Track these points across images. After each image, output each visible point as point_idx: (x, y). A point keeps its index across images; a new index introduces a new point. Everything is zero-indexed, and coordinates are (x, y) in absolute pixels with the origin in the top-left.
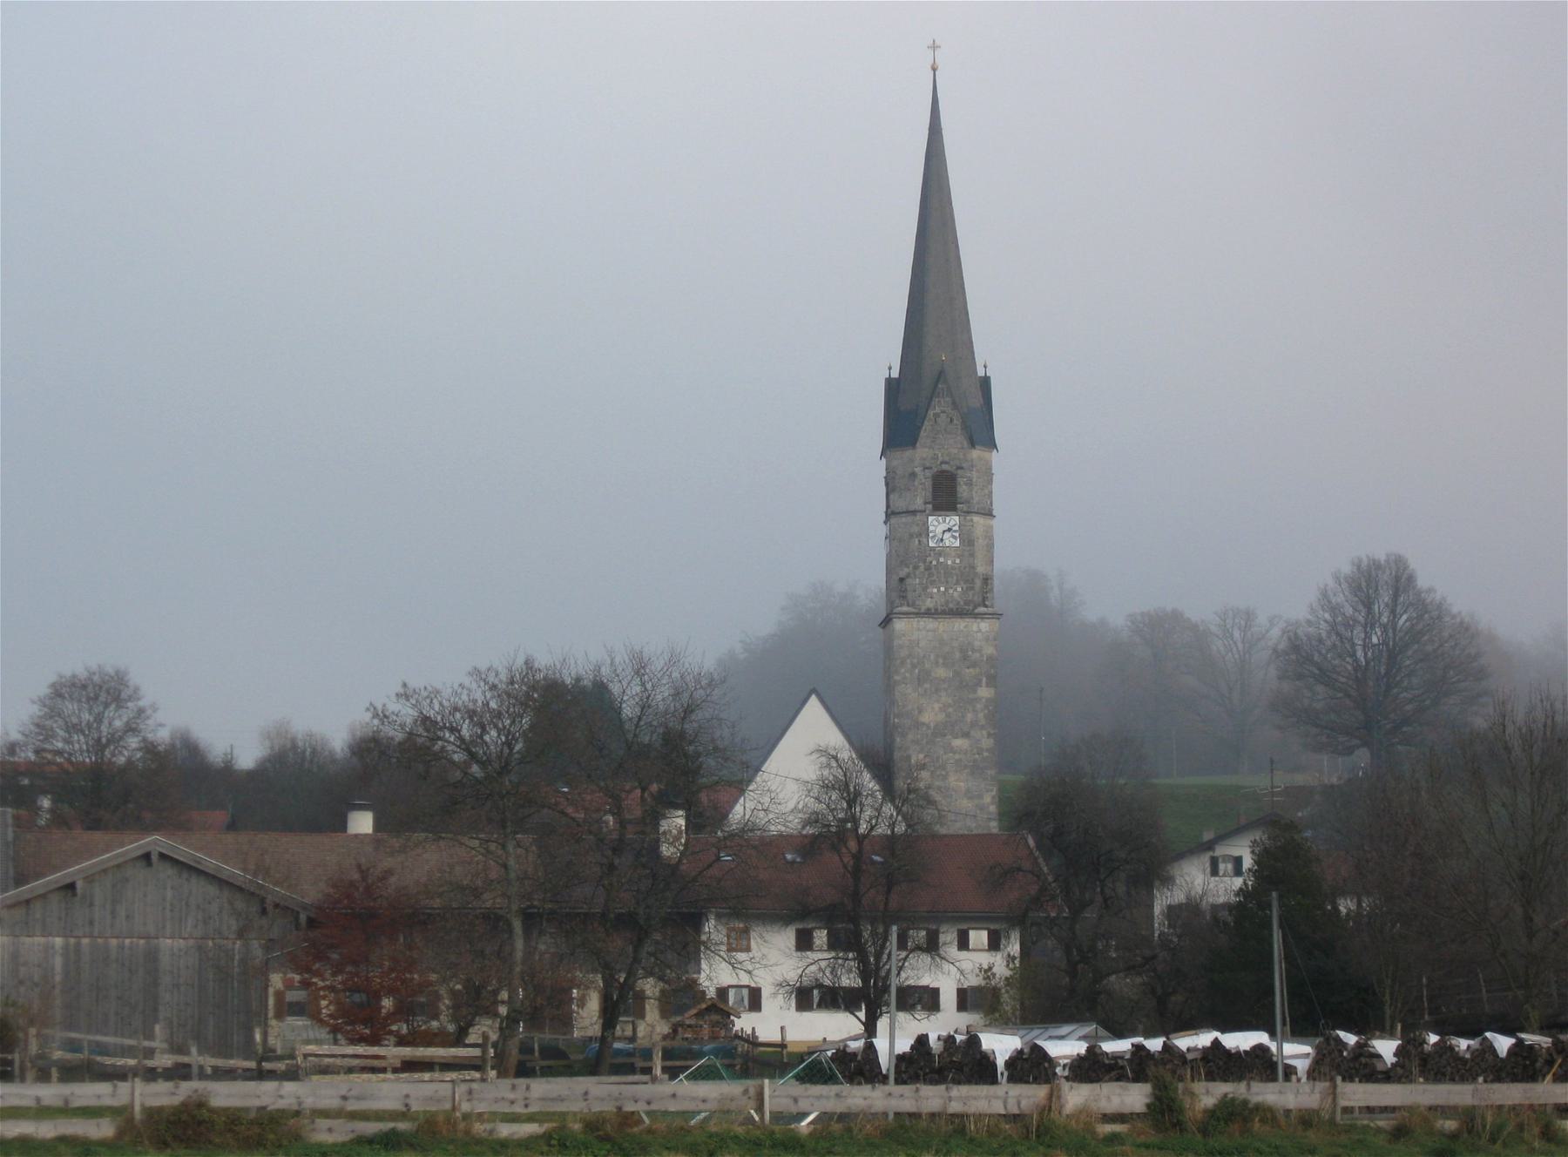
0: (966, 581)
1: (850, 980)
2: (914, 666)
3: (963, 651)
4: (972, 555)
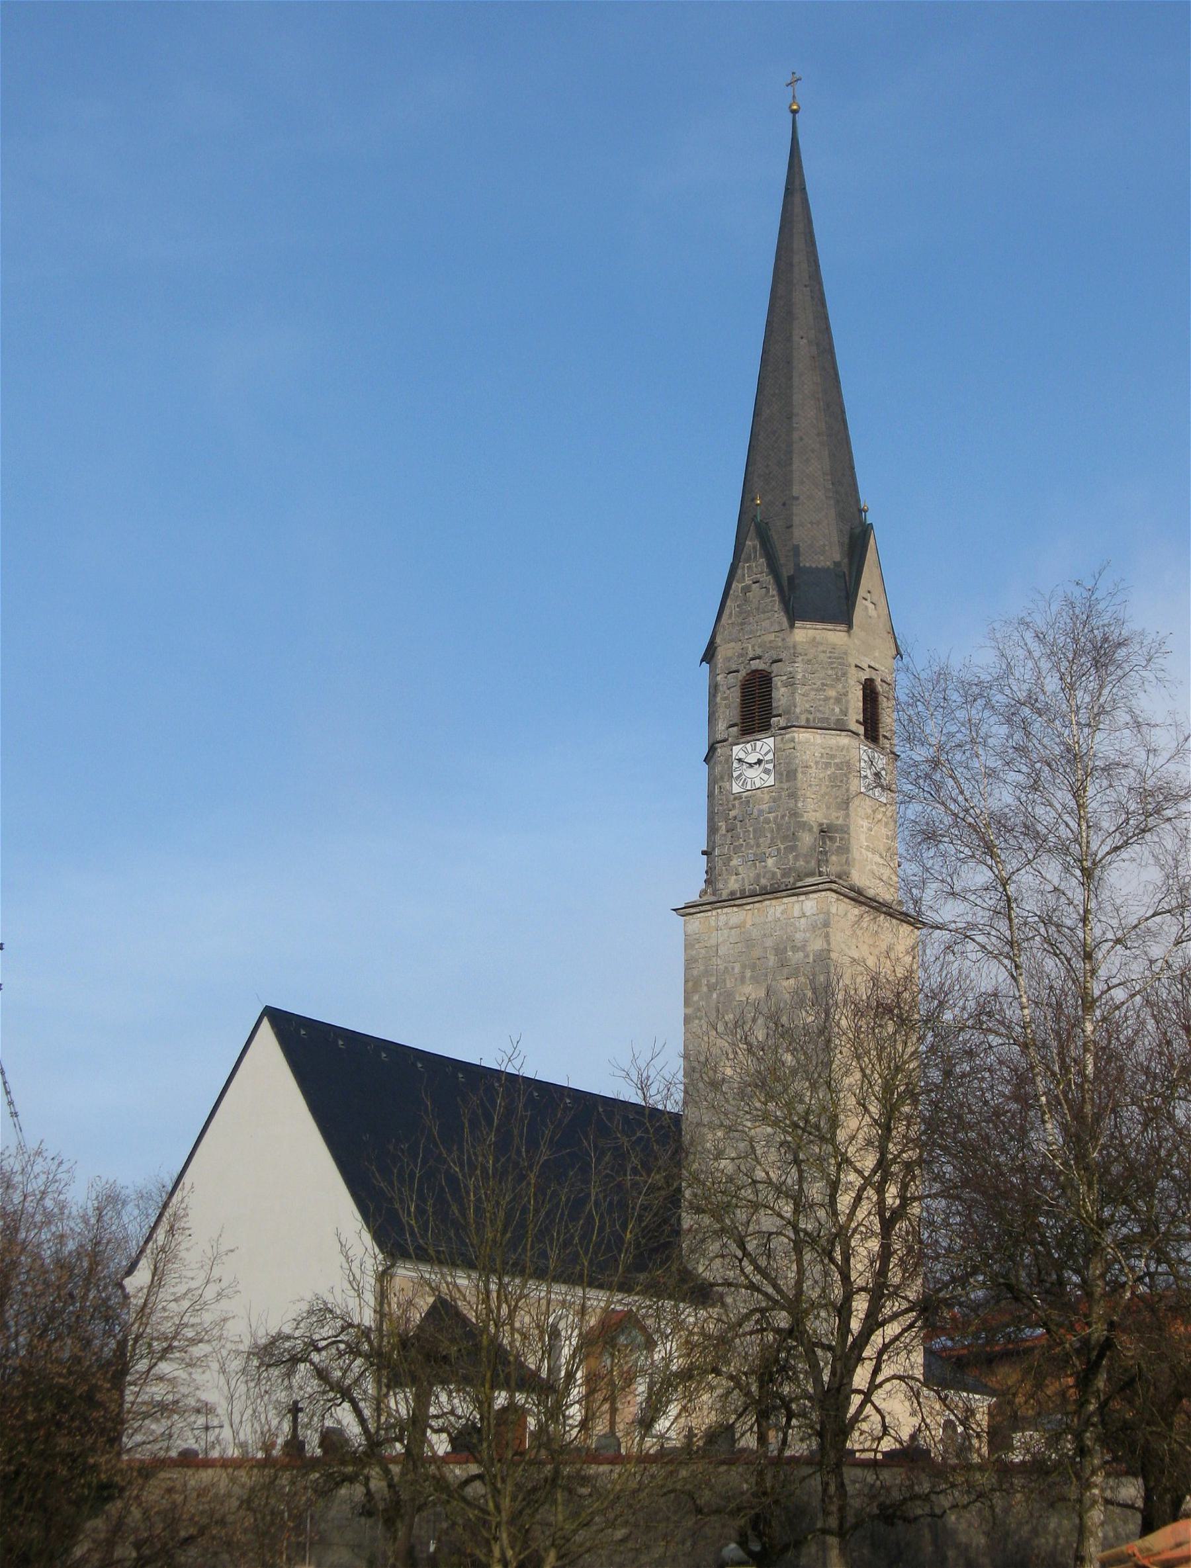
0: (785, 838)
1: (847, 1525)
2: (712, 988)
3: (780, 951)
4: (793, 795)
